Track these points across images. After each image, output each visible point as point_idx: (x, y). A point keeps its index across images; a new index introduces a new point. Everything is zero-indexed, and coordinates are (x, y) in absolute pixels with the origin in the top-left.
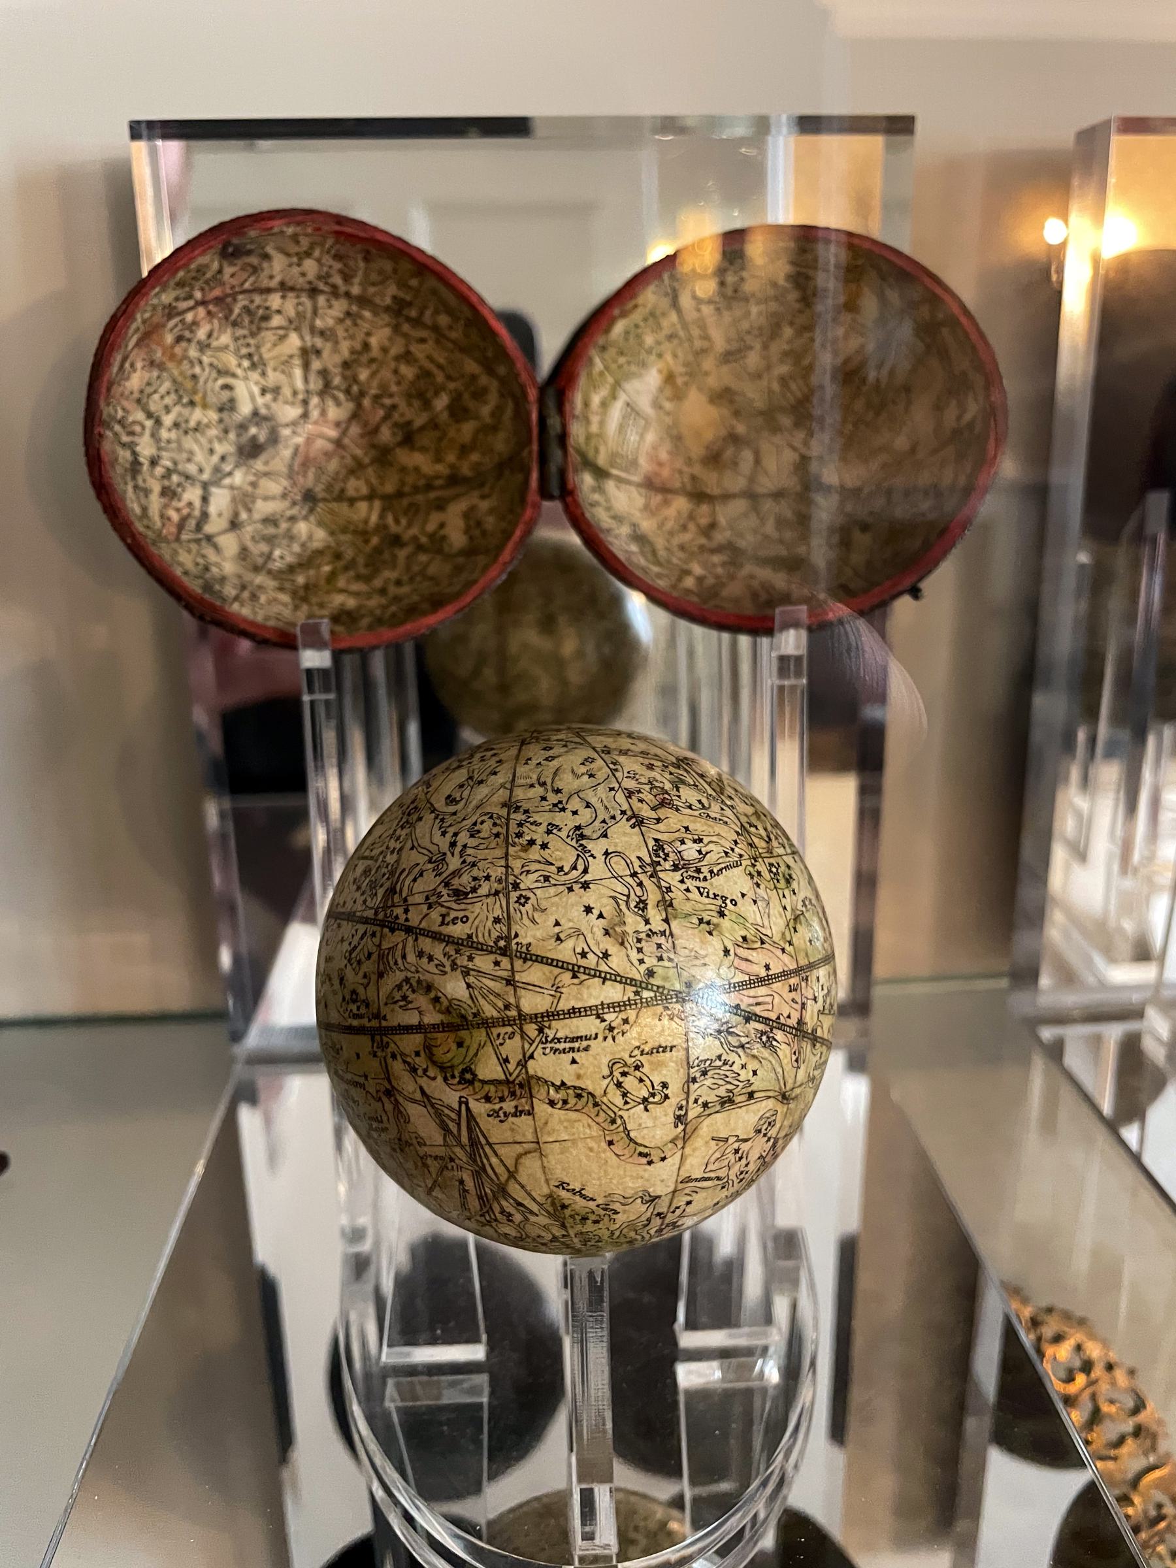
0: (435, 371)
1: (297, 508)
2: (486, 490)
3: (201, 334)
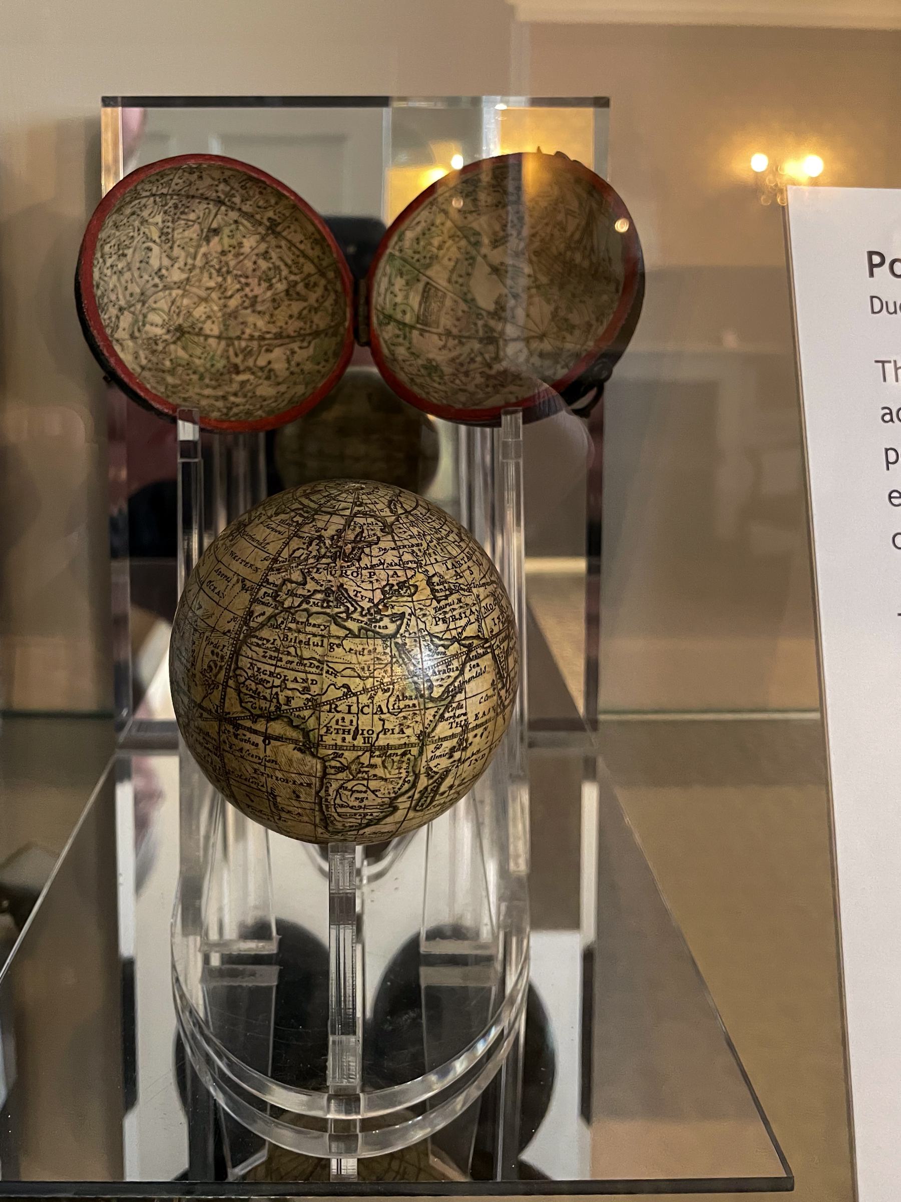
0: (283, 267)
1: (171, 334)
2: (305, 344)
3: (145, 214)
